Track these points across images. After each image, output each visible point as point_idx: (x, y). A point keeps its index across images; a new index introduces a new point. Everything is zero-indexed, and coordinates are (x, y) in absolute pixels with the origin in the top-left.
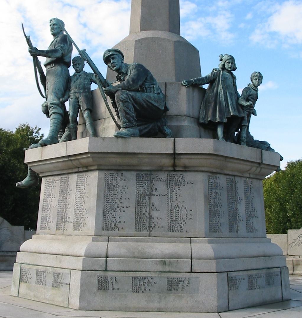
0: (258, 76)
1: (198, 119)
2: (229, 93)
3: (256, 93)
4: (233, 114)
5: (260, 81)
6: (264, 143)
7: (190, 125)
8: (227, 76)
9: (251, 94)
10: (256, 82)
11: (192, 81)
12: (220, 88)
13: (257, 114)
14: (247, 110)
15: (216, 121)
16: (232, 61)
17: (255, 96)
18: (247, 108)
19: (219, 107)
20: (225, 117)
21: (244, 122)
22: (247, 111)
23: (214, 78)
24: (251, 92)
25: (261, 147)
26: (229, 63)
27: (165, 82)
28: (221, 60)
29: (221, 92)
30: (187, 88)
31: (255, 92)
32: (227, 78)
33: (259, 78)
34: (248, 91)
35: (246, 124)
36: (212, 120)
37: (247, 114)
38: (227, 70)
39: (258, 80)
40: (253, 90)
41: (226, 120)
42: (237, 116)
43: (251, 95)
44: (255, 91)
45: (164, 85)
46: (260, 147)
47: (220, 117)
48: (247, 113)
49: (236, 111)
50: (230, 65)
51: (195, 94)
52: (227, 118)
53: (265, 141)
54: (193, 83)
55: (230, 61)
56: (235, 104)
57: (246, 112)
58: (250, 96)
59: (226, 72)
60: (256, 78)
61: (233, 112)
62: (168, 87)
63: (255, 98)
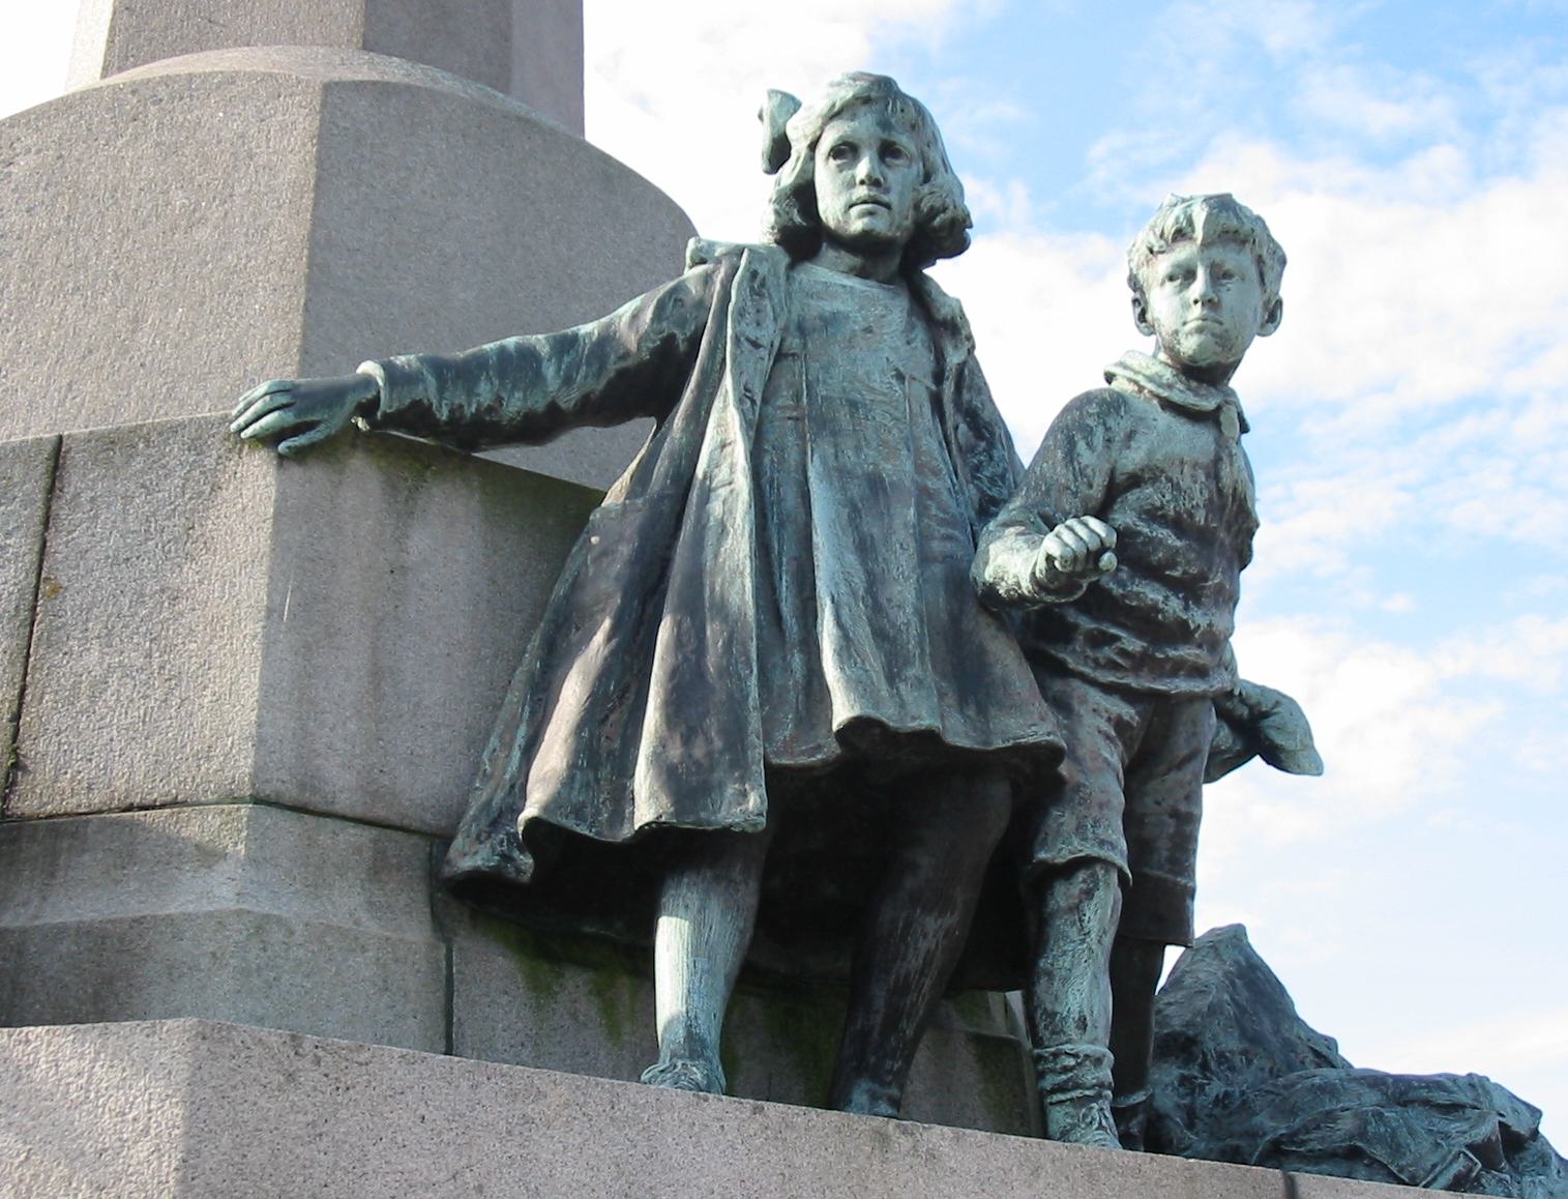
0: (1199, 234)
1: (440, 839)
2: (840, 475)
3: (1206, 458)
4: (856, 712)
5: (1230, 294)
6: (1442, 1098)
7: (292, 907)
8: (838, 306)
9: (1132, 459)
10: (1186, 306)
11: (368, 381)
12: (726, 423)
13: (1322, 742)
14: (1109, 677)
15: (626, 832)
16: (885, 125)
17: (1198, 494)
18: (1108, 652)
19: (678, 642)
20: (739, 764)
21: (1062, 819)
22: (1108, 689)
23: (672, 338)
24: (1130, 436)
25: (1397, 1150)
26: (845, 151)
27: (52, 435)
28: (779, 152)
29: (722, 474)
30: (295, 471)
31: (1193, 441)
32: (830, 321)
33: (1217, 254)
34: (1089, 432)
35: (1090, 850)
36: (570, 823)
37: (1120, 725)
38: (839, 241)
39: (1201, 273)
40: (1165, 419)
41: (755, 800)
42: (929, 737)
43: (1135, 481)
44: (1182, 428)
45: (40, 470)
46: (1380, 1153)
47: (671, 777)
48: (1127, 712)
49: (913, 671)
50: (863, 168)
51: (420, 541)
52: (776, 777)
53: (1461, 1071)
54: (377, 399)
55: (861, 127)
56: (904, 592)
57: (1096, 696)
58: (1132, 496)
59: (833, 267)
60: (1183, 252)
61: (859, 685)
62: (75, 481)
63: (1200, 517)
